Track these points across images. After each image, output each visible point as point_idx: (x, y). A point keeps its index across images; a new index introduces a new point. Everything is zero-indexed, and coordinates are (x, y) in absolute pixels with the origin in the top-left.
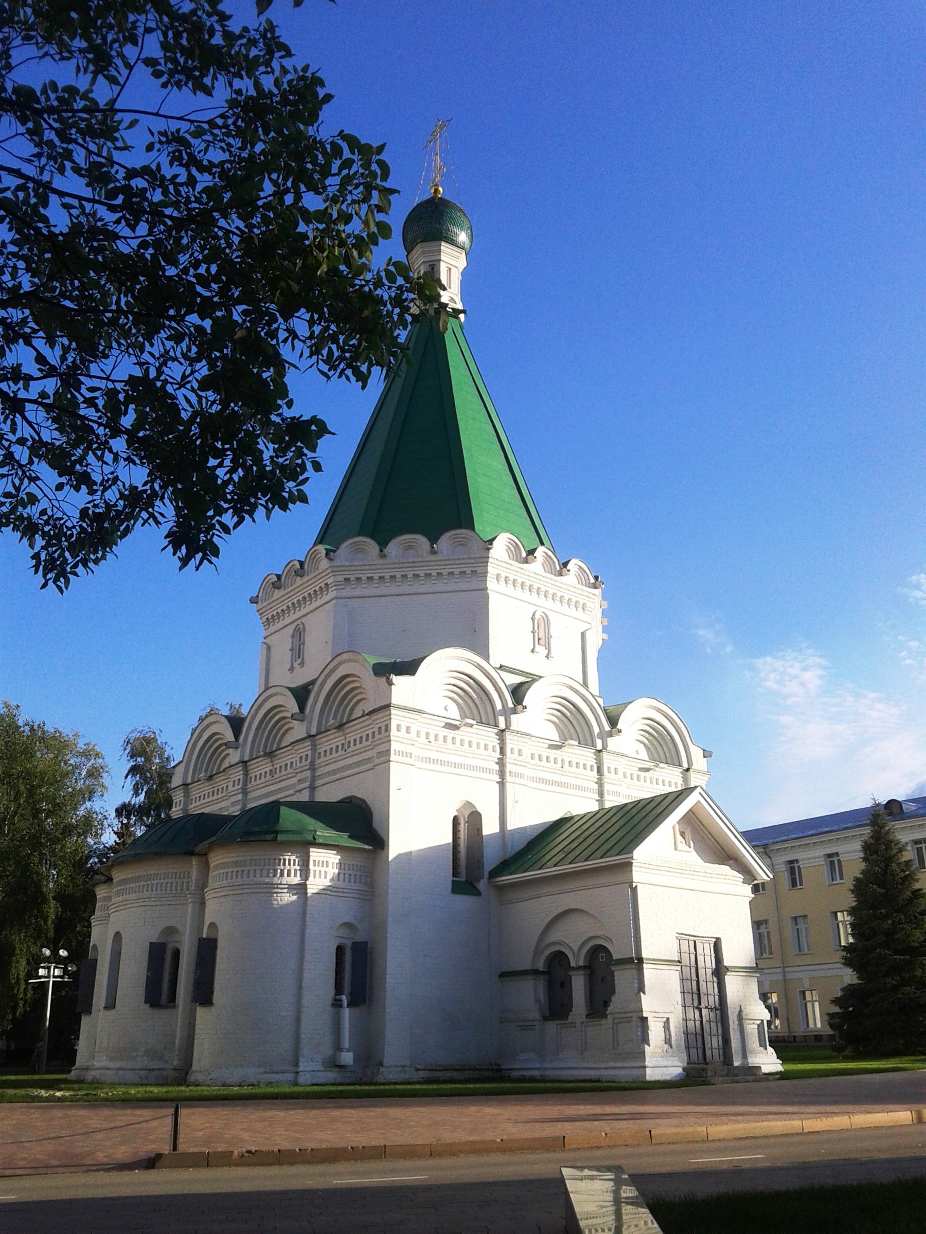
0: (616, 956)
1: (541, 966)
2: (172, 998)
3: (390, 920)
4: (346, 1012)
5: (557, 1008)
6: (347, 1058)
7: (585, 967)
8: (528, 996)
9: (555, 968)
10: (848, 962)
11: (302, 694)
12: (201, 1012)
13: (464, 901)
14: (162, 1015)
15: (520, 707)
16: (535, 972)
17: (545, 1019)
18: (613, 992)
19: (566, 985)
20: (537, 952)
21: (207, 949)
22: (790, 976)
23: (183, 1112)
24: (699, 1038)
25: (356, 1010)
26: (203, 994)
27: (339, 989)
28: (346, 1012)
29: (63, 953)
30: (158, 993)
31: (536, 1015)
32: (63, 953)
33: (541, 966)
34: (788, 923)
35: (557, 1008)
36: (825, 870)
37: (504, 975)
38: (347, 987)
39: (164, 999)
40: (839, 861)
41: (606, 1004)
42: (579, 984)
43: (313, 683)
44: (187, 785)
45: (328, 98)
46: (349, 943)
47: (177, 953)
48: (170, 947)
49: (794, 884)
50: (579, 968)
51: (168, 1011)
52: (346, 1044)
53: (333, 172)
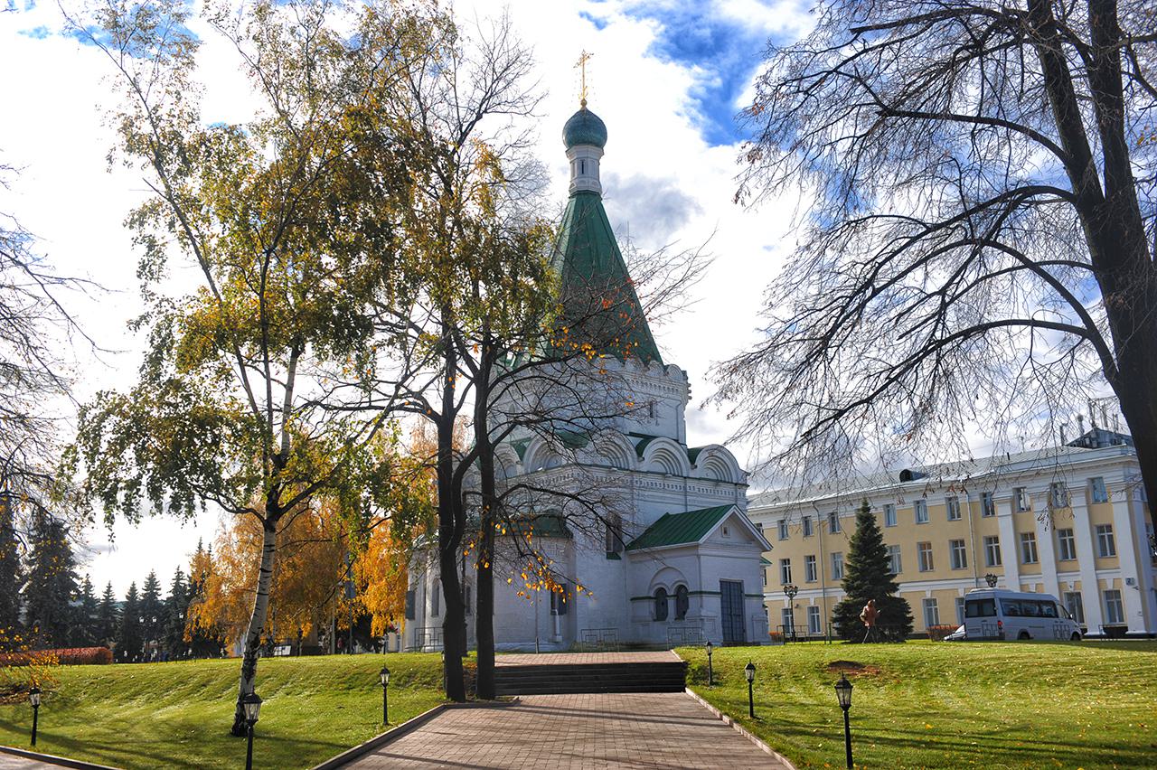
1: (652, 594)
4: (557, 617)
5: (661, 615)
6: (559, 638)
8: (648, 608)
13: (615, 563)
16: (650, 598)
18: (687, 607)
19: (665, 604)
20: (650, 588)
22: (683, 498)
27: (553, 607)
28: (557, 617)
33: (652, 594)
34: (829, 558)
35: (661, 615)
41: (684, 613)
42: (671, 603)
45: (690, 398)
47: (469, 589)
52: (558, 632)
53: (915, 631)
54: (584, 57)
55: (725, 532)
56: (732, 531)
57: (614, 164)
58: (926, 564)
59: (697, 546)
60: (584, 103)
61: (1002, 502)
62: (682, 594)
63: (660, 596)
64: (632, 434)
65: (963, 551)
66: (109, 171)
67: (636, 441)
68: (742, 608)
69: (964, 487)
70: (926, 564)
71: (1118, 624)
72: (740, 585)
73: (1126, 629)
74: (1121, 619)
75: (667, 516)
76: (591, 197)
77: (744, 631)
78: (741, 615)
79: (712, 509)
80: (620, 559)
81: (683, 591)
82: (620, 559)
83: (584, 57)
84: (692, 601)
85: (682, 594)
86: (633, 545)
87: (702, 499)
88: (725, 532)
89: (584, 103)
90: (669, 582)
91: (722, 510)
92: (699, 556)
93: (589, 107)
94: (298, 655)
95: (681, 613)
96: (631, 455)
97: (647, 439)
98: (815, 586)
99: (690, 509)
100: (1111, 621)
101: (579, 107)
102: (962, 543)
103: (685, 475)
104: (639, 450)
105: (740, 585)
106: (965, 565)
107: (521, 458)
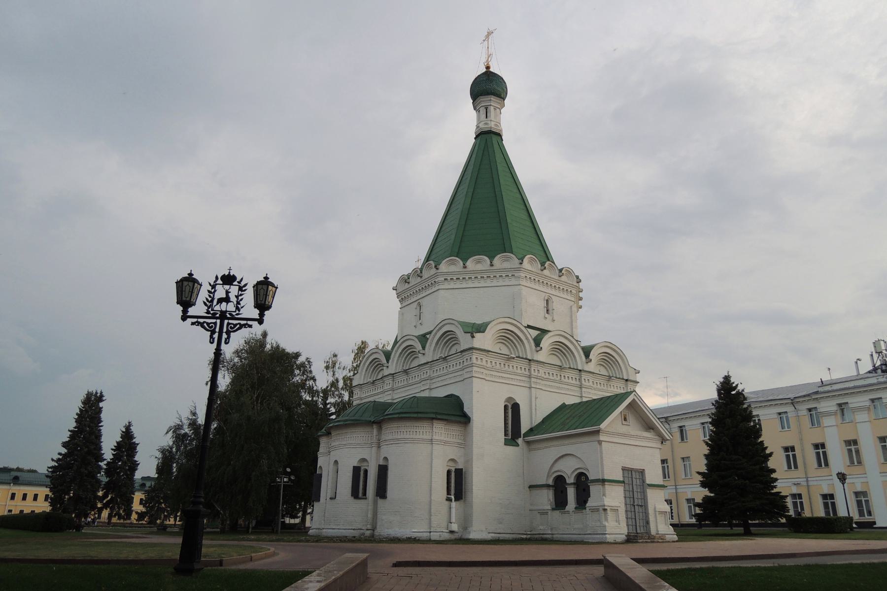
0: (591, 477)
2: (365, 494)
3: (474, 458)
4: (454, 504)
5: (560, 503)
7: (574, 484)
8: (546, 498)
9: (559, 485)
10: (703, 485)
11: (423, 339)
12: (380, 502)
13: (511, 449)
14: (360, 503)
15: (538, 348)
16: (548, 486)
17: (553, 509)
21: (383, 471)
23: (648, 482)
24: (598, 538)
25: (458, 503)
26: (382, 492)
27: (449, 492)
29: (288, 470)
30: (357, 492)
31: (549, 507)
32: (288, 470)
33: (550, 482)
36: (778, 421)
37: (531, 487)
38: (453, 492)
39: (360, 495)
40: (787, 417)
41: (586, 502)
42: (571, 493)
43: (430, 333)
44: (581, 388)
46: (453, 469)
47: (366, 471)
48: (362, 468)
49: (682, 439)
50: (571, 484)
51: (362, 501)
52: (453, 520)
54: (489, 34)
55: (625, 419)
56: (631, 419)
57: (513, 120)
58: (792, 462)
59: (598, 432)
60: (488, 68)
61: (828, 414)
62: (583, 484)
63: (559, 485)
64: (529, 327)
65: (794, 456)
66: (335, 356)
67: (535, 333)
68: (645, 498)
69: (793, 402)
70: (792, 462)
71: (867, 518)
72: (642, 472)
73: (874, 523)
74: (870, 513)
75: (563, 407)
76: (493, 136)
77: (648, 523)
78: (644, 506)
79: (617, 395)
80: (518, 445)
81: (583, 479)
82: (518, 445)
83: (489, 34)
84: (594, 489)
85: (583, 484)
86: (531, 431)
87: (595, 391)
88: (625, 419)
89: (488, 68)
90: (569, 470)
91: (618, 399)
92: (600, 442)
93: (491, 70)
94: (277, 532)
95: (582, 500)
96: (530, 346)
97: (544, 332)
98: (691, 482)
99: (585, 400)
100: (860, 516)
101: (485, 70)
102: (793, 449)
103: (580, 368)
104: (537, 342)
105: (642, 472)
106: (796, 467)
107: (424, 348)
